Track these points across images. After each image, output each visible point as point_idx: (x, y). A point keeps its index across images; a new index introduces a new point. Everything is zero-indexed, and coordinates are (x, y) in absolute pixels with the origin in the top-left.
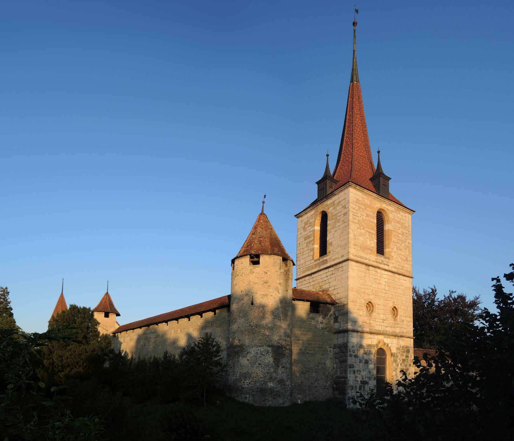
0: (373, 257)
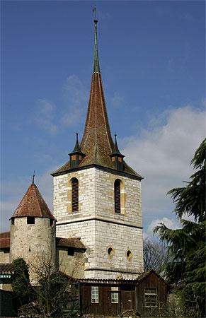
0: (113, 216)
